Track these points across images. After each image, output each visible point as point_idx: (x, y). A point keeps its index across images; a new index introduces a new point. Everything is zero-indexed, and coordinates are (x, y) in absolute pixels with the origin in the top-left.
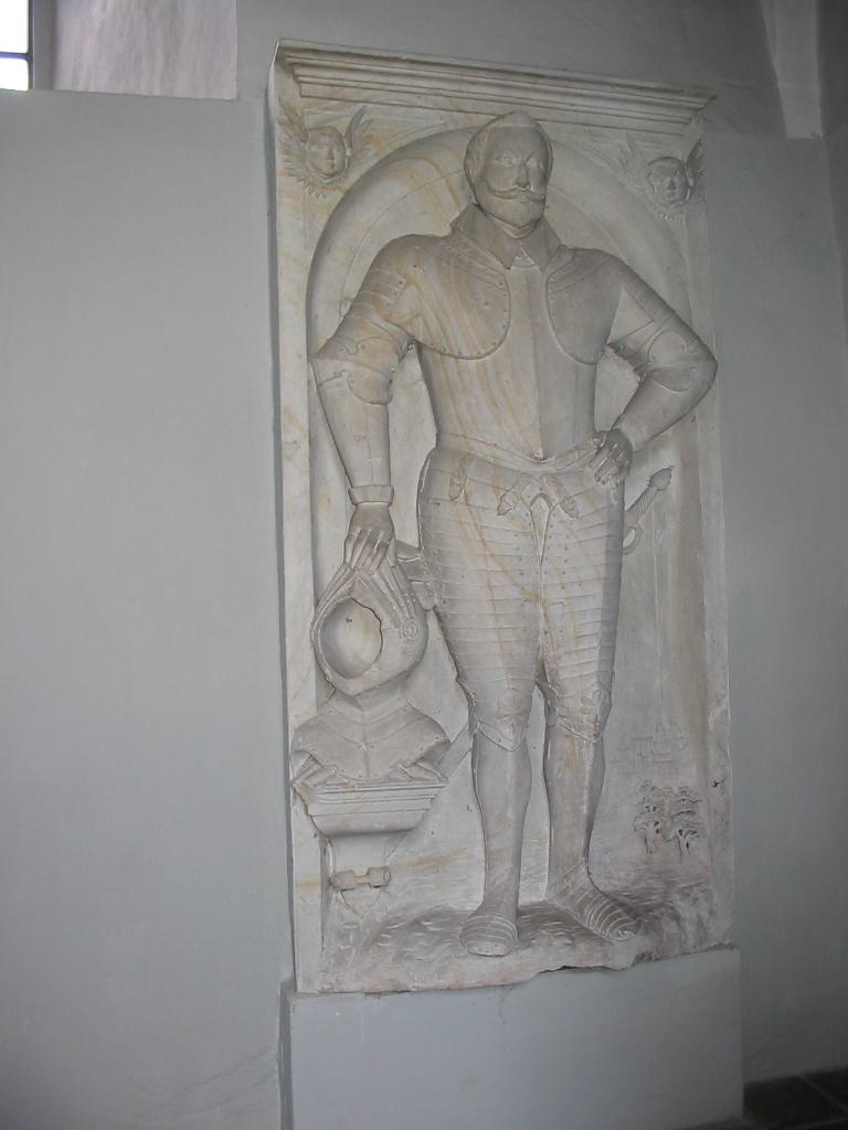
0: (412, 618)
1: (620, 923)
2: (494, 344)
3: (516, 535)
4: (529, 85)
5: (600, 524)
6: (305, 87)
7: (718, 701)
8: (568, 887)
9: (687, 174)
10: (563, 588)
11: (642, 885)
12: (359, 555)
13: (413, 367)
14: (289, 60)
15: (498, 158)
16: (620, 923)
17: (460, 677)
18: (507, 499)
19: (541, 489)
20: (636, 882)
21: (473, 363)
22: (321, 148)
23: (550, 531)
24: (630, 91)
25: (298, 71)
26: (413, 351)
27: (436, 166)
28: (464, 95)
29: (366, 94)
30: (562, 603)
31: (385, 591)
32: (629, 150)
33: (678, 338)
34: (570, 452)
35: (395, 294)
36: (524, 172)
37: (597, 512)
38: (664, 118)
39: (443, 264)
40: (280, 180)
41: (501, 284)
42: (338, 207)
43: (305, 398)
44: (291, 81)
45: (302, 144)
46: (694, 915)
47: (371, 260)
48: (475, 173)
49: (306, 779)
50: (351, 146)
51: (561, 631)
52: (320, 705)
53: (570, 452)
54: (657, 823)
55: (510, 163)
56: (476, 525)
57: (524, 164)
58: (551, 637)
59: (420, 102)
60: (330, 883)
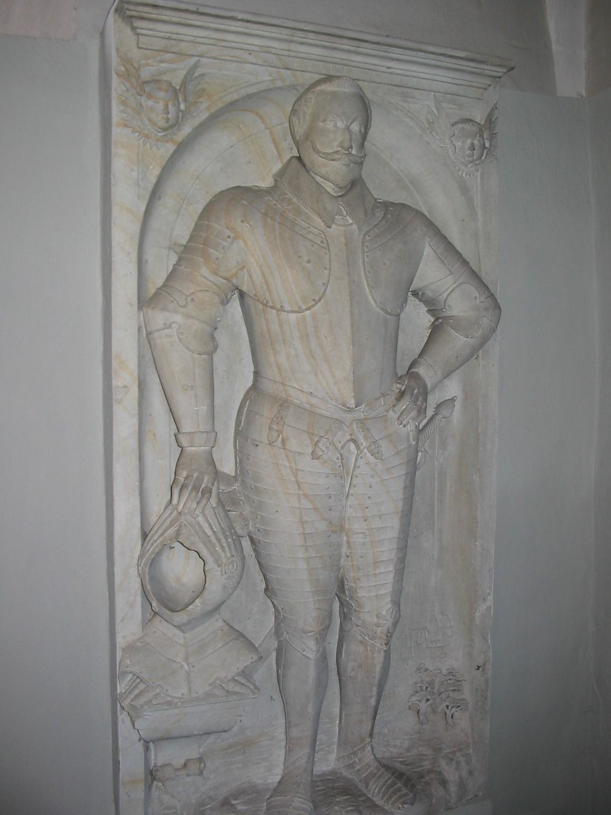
0: (233, 556)
1: (400, 797)
2: (314, 300)
3: (327, 477)
4: (352, 49)
5: (400, 464)
6: (142, 39)
7: (484, 599)
8: (354, 762)
9: (485, 136)
10: (365, 520)
11: (415, 751)
12: (185, 501)
13: (235, 307)
14: (128, 13)
15: (324, 121)
16: (400, 797)
17: (268, 591)
18: (321, 445)
19: (351, 435)
20: (408, 750)
21: (293, 317)
22: (158, 103)
23: (357, 472)
24: (441, 57)
25: (138, 24)
26: (236, 296)
27: (261, 118)
28: (293, 54)
29: (201, 49)
30: (364, 533)
31: (209, 532)
32: (435, 110)
33: (472, 290)
34: (376, 399)
35: (224, 248)
36: (347, 136)
37: (398, 453)
38: (468, 83)
39: (269, 220)
40: (116, 131)
41: (322, 242)
42: (213, 381)
43: (135, 344)
44: (129, 31)
45: (139, 97)
46: (457, 776)
47: (200, 208)
48: (300, 130)
49: (132, 701)
50: (185, 100)
51: (362, 557)
52: (146, 623)
53: (376, 399)
54: (428, 700)
55: (335, 126)
56: (291, 468)
57: (348, 128)
58: (352, 561)
59: (251, 59)
60: (152, 775)
